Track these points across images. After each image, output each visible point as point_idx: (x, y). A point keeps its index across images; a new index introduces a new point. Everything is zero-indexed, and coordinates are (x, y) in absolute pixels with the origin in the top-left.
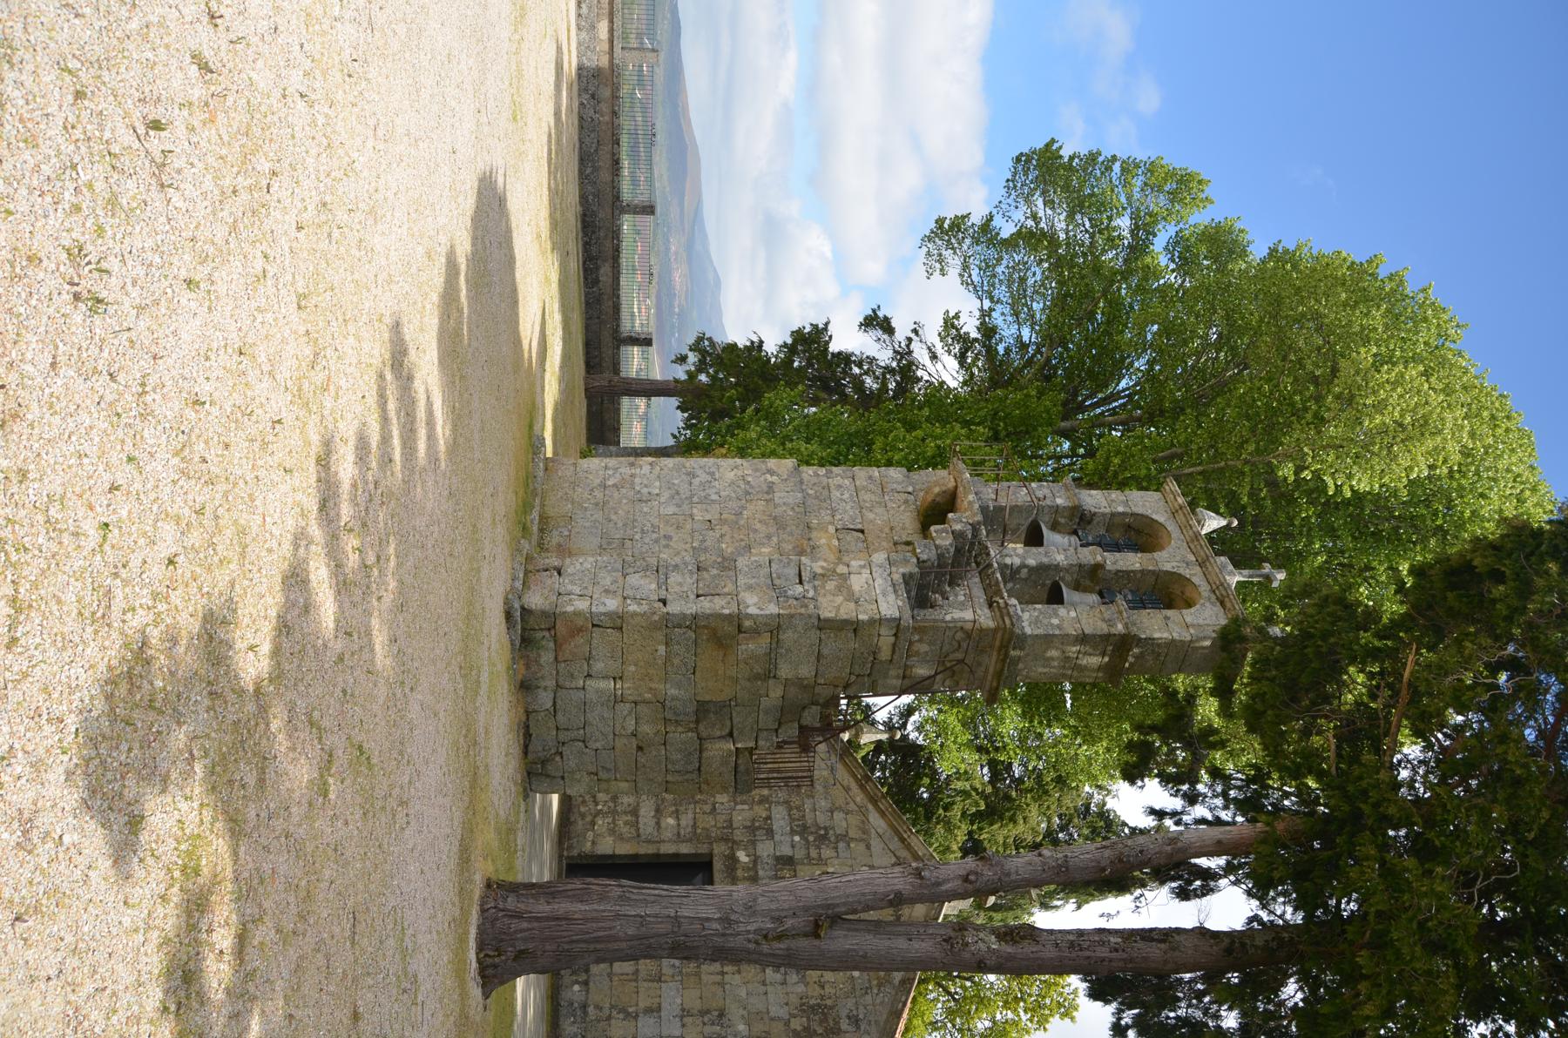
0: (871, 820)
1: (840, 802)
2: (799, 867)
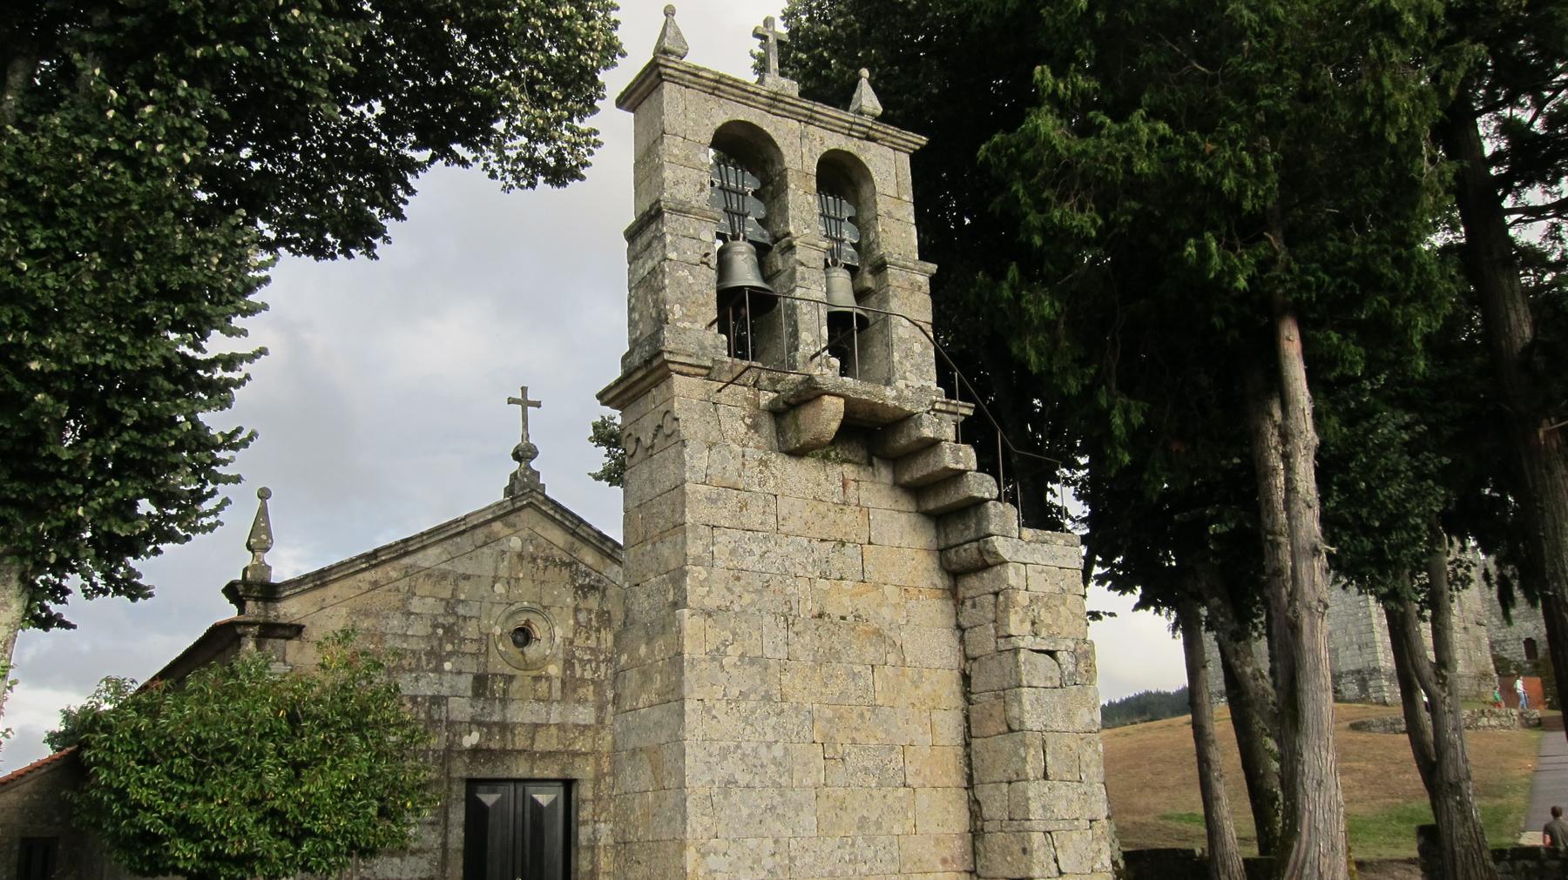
0: (427, 564)
1: (394, 600)
2: (490, 670)
